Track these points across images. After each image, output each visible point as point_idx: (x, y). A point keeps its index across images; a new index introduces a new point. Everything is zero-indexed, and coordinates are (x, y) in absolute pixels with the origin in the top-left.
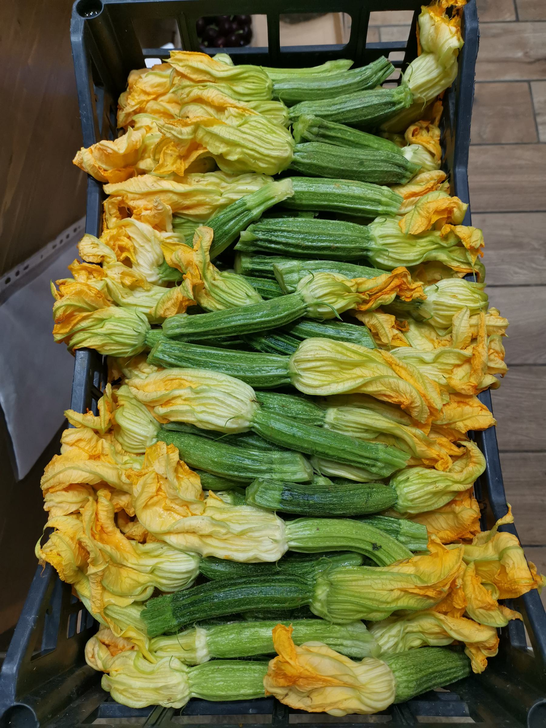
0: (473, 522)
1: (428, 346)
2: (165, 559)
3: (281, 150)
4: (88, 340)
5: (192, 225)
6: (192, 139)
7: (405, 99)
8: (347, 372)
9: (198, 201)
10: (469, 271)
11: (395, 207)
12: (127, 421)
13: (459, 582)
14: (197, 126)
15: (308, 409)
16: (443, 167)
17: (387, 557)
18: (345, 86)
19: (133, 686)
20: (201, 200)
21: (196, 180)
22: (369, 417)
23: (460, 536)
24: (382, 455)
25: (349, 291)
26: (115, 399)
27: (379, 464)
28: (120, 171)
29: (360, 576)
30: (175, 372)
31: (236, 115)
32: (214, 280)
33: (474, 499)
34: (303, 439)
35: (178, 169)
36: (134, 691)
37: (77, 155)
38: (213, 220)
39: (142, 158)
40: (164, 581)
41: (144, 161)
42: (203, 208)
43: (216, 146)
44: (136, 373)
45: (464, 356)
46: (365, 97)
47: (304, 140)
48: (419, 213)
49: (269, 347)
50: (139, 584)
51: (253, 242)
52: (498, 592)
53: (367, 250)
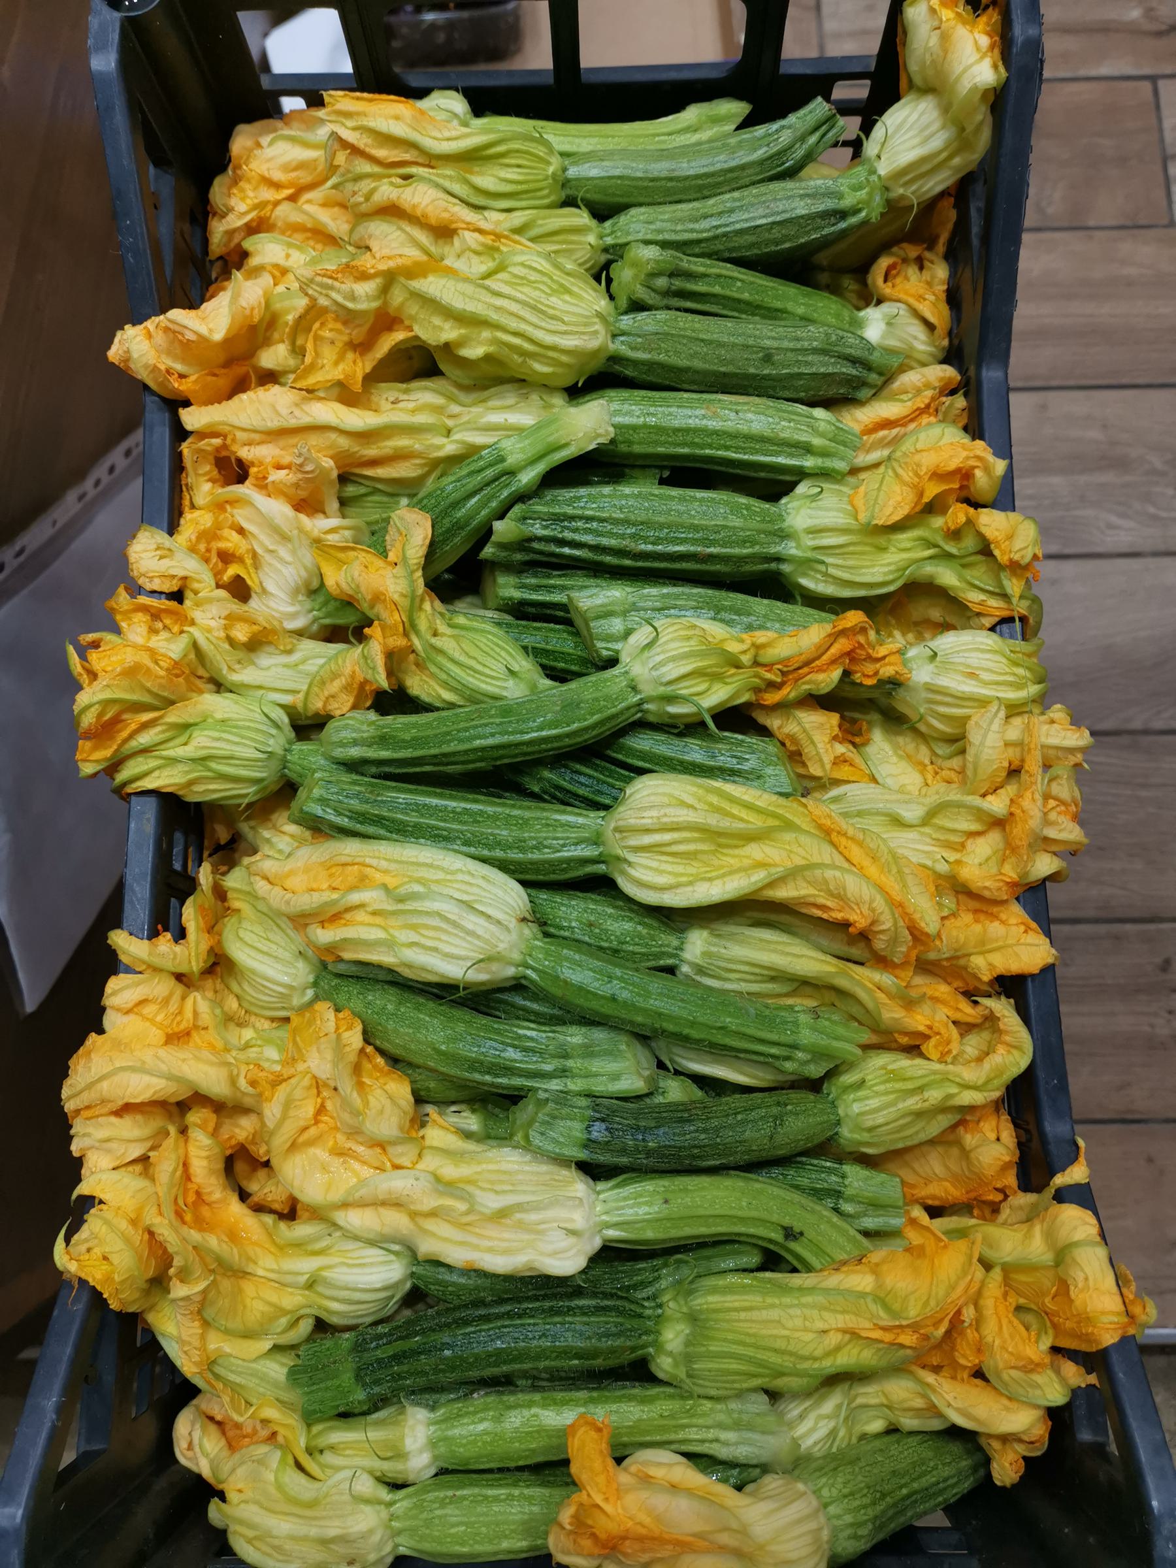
0: (1005, 1167)
1: (911, 779)
2: (337, 1260)
3: (584, 333)
4: (156, 774)
5: (385, 499)
6: (378, 309)
7: (868, 203)
8: (730, 851)
9: (396, 449)
10: (1006, 614)
11: (842, 459)
12: (247, 950)
13: (969, 1314)
14: (390, 278)
15: (645, 931)
16: (951, 356)
17: (817, 1255)
18: (731, 170)
19: (275, 1532)
20: (402, 448)
21: (391, 399)
22: (780, 947)
23: (973, 1195)
24: (806, 1036)
25: (738, 666)
26: (220, 894)
27: (800, 1055)
28: (215, 375)
29: (754, 1299)
30: (351, 848)
31: (480, 248)
32: (435, 634)
33: (1005, 1117)
34: (633, 1005)
35: (347, 376)
36: (276, 1542)
37: (116, 340)
38: (429, 495)
39: (267, 342)
40: (335, 1306)
41: (272, 349)
42: (407, 464)
43: (435, 327)
44: (266, 834)
45: (989, 814)
46: (775, 199)
47: (637, 306)
48: (897, 475)
49: (558, 788)
50: (284, 1312)
51: (524, 544)
52: (1051, 1332)
53: (778, 559)
